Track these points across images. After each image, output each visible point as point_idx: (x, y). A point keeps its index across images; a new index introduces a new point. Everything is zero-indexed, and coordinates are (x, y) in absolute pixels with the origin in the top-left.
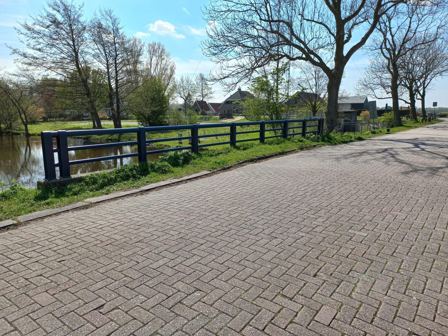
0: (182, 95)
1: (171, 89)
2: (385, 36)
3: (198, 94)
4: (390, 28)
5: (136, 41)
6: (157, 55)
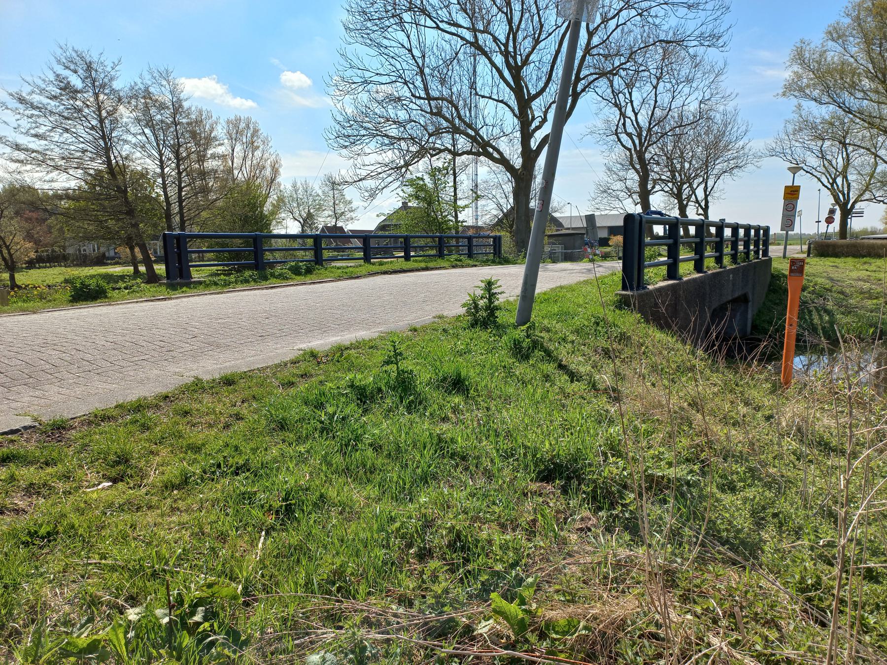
0: (297, 215)
1: (273, 205)
2: (623, 115)
3: (326, 213)
4: (631, 102)
5: (202, 115)
6: (244, 140)
